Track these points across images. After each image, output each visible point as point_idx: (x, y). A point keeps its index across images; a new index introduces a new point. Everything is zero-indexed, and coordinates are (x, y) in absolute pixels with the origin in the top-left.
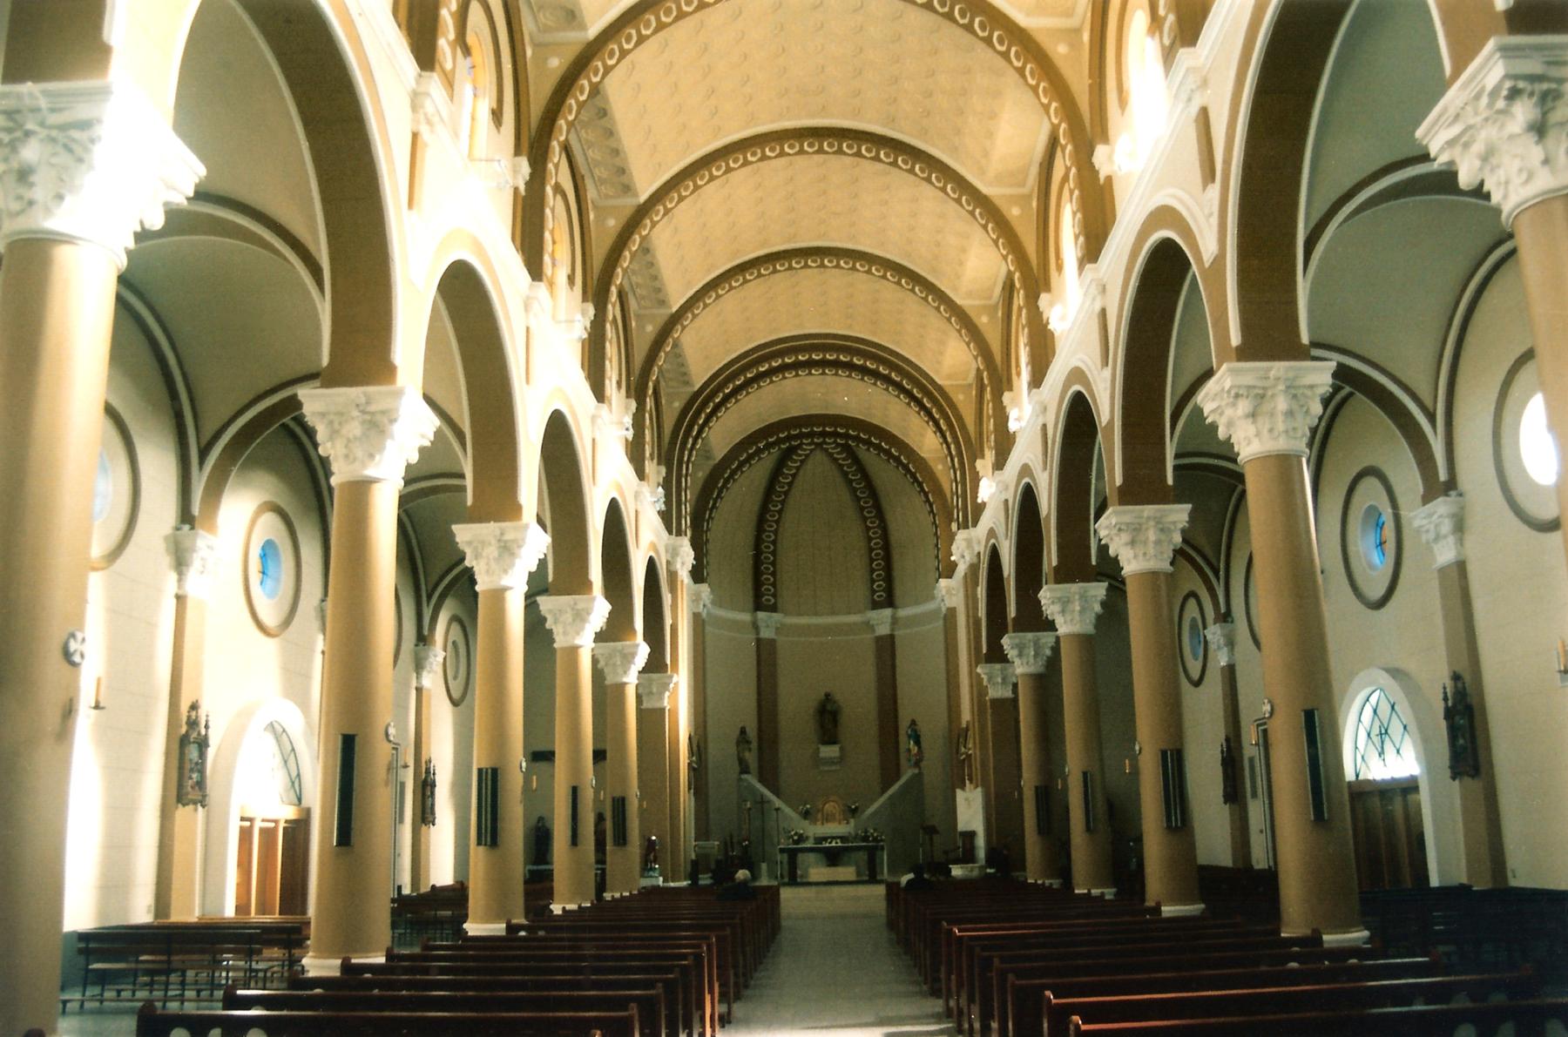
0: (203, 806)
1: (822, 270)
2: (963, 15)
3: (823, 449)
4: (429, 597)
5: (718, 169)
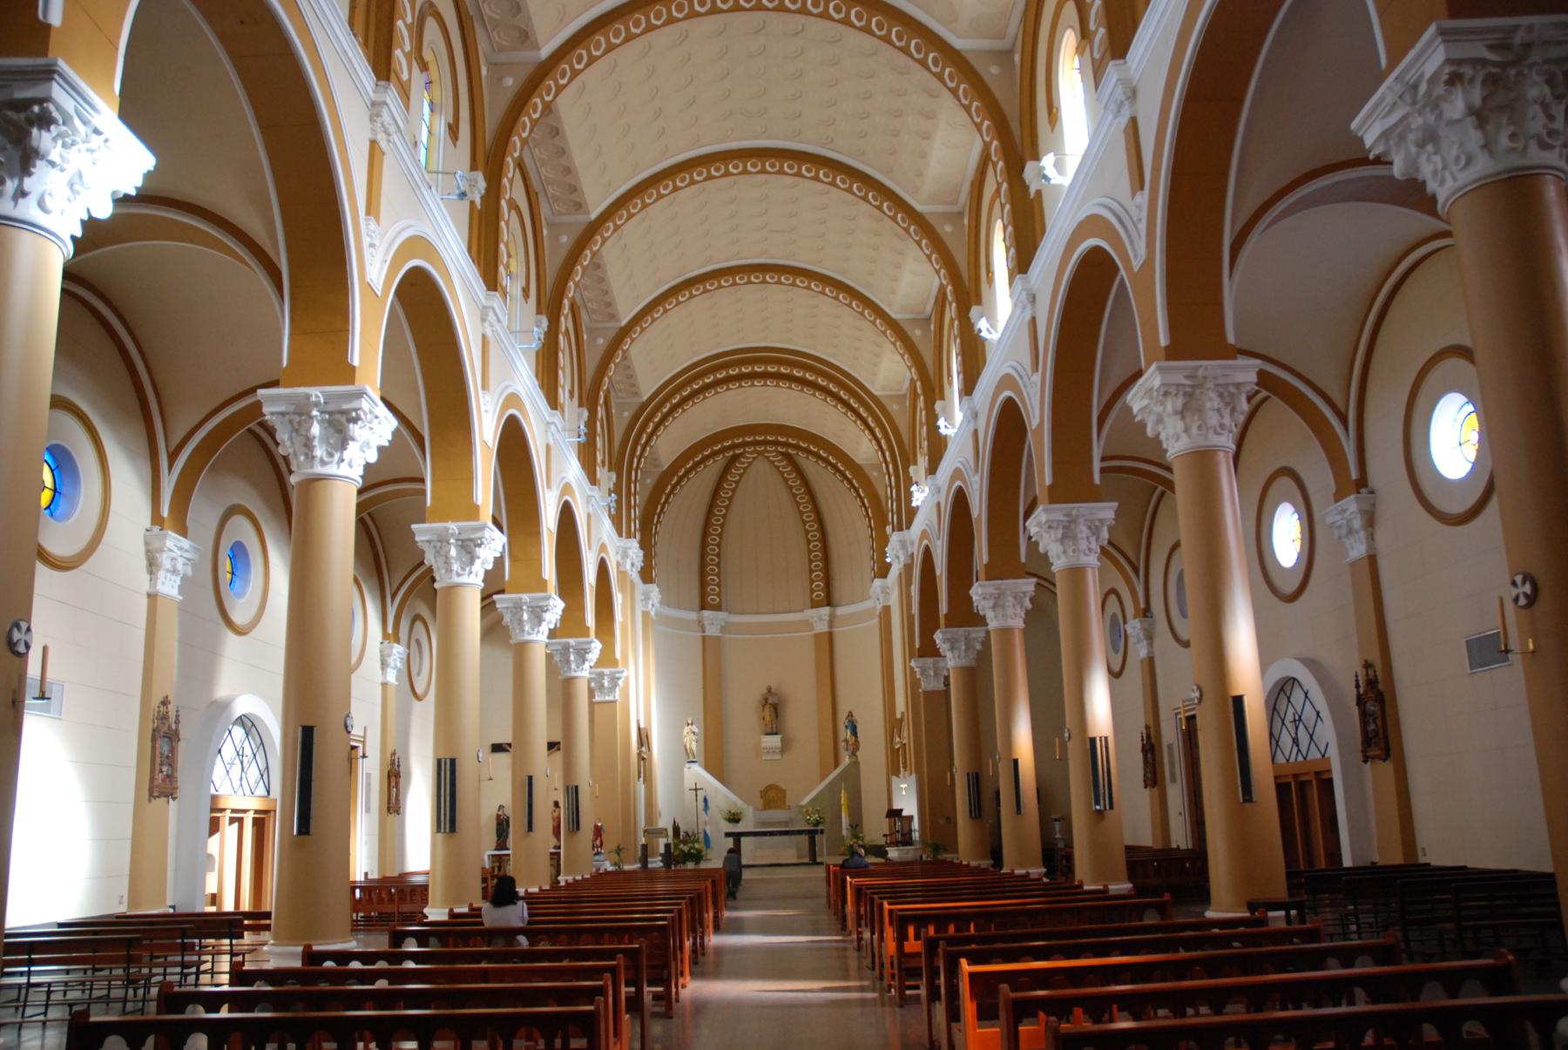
0: (174, 799)
2: (900, 38)
3: (763, 455)
4: (393, 597)
5: (666, 188)
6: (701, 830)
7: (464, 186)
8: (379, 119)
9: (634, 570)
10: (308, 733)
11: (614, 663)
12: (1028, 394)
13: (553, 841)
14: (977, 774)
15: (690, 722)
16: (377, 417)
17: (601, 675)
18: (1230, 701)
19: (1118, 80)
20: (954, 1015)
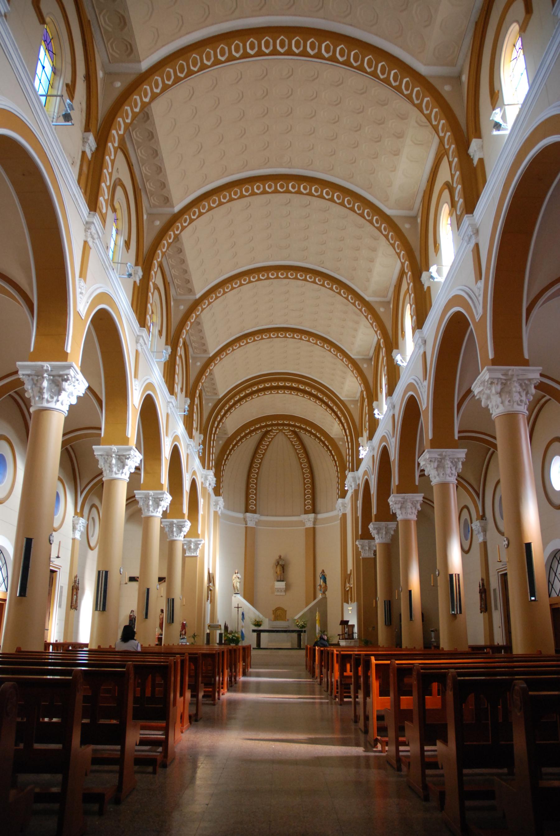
1: (286, 339)
3: (282, 432)
4: (81, 493)
6: (240, 630)
7: (131, 271)
8: (89, 231)
9: (210, 487)
10: (29, 542)
11: (197, 536)
12: (421, 392)
13: (158, 631)
14: (390, 601)
15: (237, 572)
16: (77, 380)
17: (190, 542)
18: (524, 545)
19: (469, 224)
20: (367, 694)
